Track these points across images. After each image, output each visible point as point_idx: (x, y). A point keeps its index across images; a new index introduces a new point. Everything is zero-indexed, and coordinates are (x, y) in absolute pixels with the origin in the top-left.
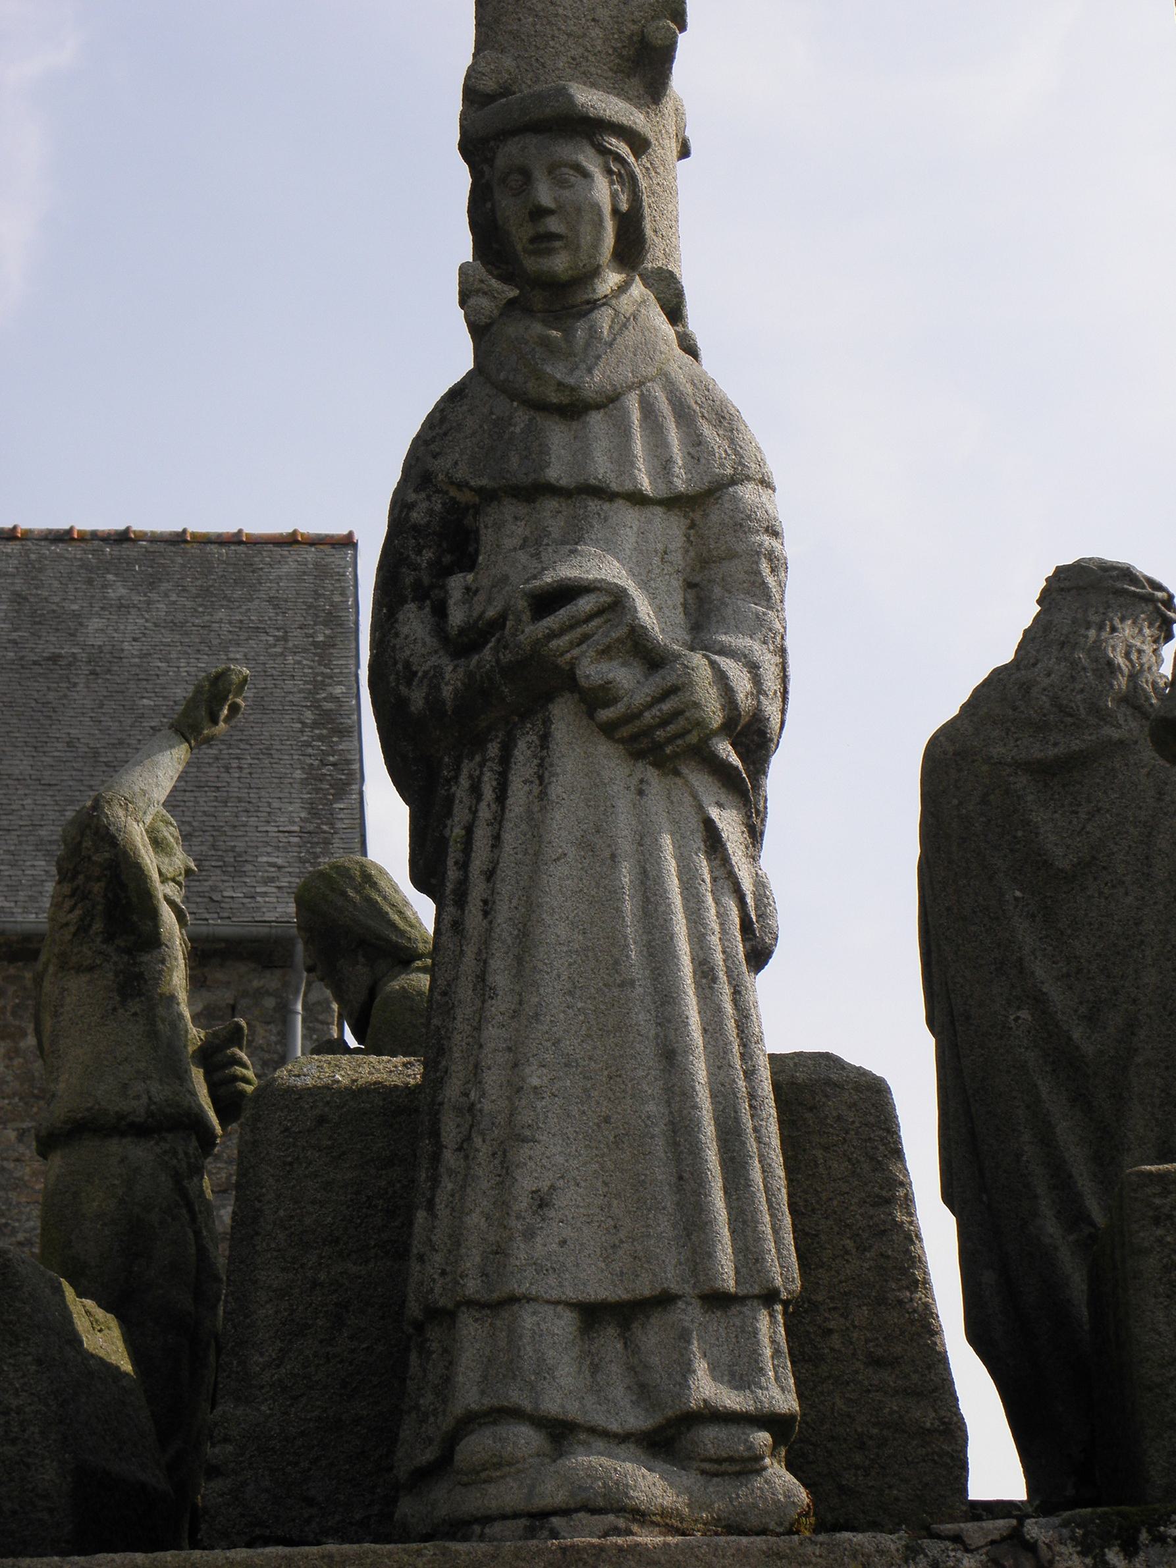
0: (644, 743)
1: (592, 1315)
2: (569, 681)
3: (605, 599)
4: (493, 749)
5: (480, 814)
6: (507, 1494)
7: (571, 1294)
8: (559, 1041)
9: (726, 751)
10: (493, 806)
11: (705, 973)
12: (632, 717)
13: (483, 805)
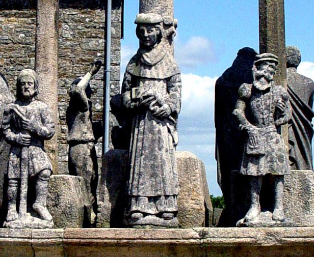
1: (150, 199)
3: (153, 97)
7: (147, 196)
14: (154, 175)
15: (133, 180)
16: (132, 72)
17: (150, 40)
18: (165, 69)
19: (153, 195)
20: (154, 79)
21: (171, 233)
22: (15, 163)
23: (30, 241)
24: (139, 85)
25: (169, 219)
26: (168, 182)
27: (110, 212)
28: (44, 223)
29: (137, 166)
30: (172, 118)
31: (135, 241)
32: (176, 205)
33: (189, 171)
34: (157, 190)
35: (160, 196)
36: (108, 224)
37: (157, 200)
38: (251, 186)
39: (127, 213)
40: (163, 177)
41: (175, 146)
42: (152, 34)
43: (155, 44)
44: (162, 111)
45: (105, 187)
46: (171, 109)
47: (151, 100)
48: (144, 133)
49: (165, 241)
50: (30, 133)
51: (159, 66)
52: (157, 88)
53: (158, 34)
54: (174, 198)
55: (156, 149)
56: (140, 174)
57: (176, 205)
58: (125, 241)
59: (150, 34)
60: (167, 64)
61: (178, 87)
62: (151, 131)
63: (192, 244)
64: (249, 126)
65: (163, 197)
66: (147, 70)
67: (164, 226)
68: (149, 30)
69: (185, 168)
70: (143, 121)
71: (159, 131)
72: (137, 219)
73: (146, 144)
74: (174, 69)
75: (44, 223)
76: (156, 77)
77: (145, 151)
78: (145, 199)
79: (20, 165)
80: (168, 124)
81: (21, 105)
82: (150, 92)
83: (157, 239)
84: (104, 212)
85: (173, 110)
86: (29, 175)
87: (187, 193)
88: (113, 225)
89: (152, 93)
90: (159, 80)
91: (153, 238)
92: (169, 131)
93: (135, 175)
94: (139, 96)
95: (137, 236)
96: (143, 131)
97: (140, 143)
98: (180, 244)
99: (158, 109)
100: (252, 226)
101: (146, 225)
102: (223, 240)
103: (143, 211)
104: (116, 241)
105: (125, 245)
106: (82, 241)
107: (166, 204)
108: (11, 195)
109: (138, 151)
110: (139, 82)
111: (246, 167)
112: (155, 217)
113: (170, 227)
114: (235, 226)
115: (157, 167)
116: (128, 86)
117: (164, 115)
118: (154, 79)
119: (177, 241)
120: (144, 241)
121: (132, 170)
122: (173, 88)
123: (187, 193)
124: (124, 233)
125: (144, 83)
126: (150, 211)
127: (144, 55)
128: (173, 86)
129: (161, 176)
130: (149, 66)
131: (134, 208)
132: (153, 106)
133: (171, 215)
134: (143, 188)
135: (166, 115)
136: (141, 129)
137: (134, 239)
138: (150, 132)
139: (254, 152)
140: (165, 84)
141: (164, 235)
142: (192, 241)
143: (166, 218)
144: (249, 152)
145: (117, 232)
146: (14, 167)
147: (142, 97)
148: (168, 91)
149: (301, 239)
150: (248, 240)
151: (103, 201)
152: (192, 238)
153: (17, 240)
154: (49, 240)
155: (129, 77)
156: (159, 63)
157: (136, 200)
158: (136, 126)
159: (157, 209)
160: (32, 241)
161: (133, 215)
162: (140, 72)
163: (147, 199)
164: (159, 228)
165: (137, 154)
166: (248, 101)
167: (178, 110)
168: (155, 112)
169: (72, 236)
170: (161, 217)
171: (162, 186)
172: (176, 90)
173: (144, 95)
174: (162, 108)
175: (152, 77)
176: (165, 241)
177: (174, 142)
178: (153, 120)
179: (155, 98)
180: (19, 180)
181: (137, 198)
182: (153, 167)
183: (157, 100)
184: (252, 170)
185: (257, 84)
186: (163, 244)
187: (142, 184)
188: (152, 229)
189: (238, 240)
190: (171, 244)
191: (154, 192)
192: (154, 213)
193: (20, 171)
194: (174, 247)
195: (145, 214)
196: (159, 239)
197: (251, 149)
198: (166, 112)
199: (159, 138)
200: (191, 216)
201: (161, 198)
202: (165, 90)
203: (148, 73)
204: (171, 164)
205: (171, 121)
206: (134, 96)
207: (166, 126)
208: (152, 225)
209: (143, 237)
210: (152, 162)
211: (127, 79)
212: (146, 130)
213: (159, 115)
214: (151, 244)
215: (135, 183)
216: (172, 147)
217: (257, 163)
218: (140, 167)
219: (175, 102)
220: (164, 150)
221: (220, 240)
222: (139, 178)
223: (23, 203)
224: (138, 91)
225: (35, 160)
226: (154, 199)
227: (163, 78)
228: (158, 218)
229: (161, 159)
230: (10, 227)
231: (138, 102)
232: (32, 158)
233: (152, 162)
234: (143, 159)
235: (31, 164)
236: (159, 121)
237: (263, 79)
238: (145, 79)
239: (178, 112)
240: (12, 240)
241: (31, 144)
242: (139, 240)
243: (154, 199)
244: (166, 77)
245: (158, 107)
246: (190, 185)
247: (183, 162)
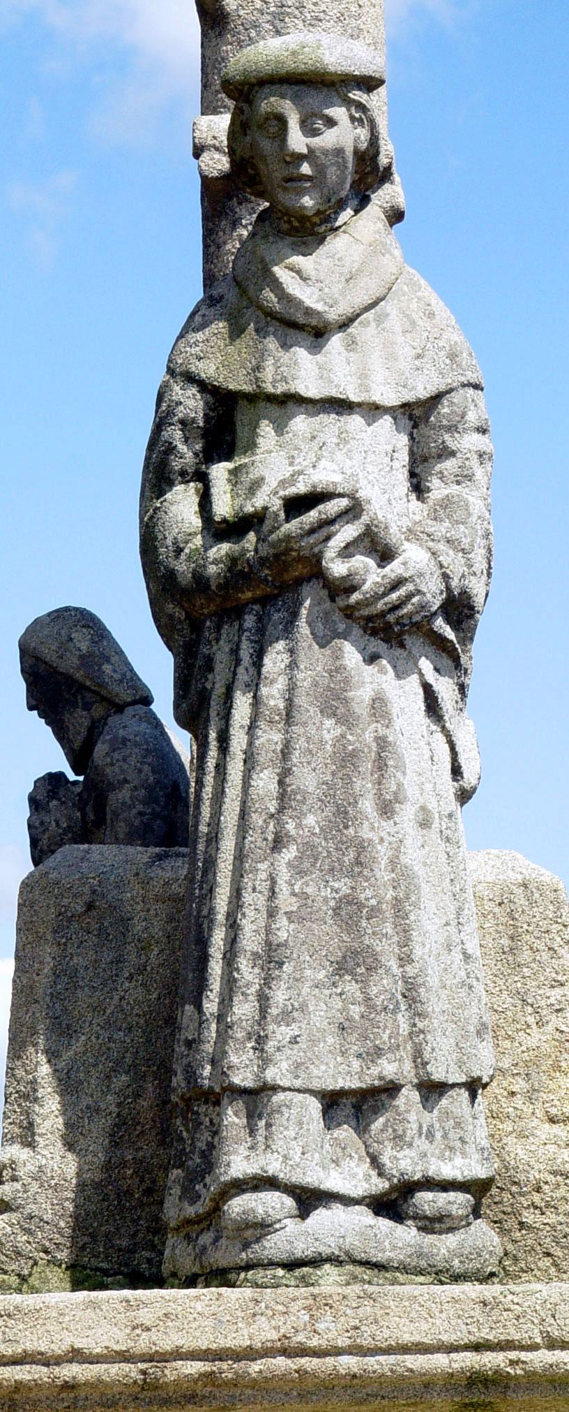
0: (379, 623)
1: (332, 1102)
2: (317, 572)
3: (344, 503)
4: (249, 621)
5: (239, 676)
6: (274, 1246)
7: (316, 1085)
8: (427, 1063)
9: (441, 625)
10: (251, 670)
11: (240, 856)
12: (367, 603)
13: (241, 670)
14: (353, 963)
15: (232, 1001)
16: (208, 369)
17: (317, 180)
18: (405, 352)
19: (354, 1084)
20: (340, 406)
21: (477, 1312)
24: (251, 446)
25: (451, 1230)
26: (436, 1003)
27: (70, 1206)
29: (250, 912)
30: (450, 634)
31: (255, 1367)
32: (485, 1143)
33: (526, 956)
34: (378, 1052)
35: (391, 1089)
36: (57, 1275)
37: (376, 1111)
39: (190, 1195)
40: (410, 970)
41: (464, 796)
42: (328, 139)
43: (341, 205)
44: (397, 584)
45: (42, 1058)
46: (446, 577)
47: (331, 522)
48: (289, 714)
49: (440, 1361)
51: (372, 330)
52: (358, 457)
53: (363, 146)
54: (473, 1096)
55: (368, 805)
56: (271, 957)
57: (485, 1143)
58: (194, 1368)
59: (316, 141)
60: (413, 323)
61: (474, 462)
62: (335, 701)
65: (409, 1097)
66: (301, 353)
67: (421, 1272)
68: (314, 115)
69: (505, 942)
70: (280, 645)
71: (379, 707)
72: (263, 1227)
73: (307, 779)
74: (453, 356)
76: (354, 398)
77: (300, 817)
78: (303, 1106)
80: (426, 665)
82: (324, 475)
83: (388, 1351)
84: (31, 1208)
85: (454, 583)
87: (519, 1085)
88: (85, 1276)
89: (337, 478)
90: (373, 410)
91: (366, 1342)
92: (432, 705)
93: (243, 963)
94: (260, 500)
95: (265, 1332)
96: (282, 705)
97: (265, 774)
98: (530, 1375)
99: (371, 574)
101: (315, 1262)
103: (297, 1178)
104: (132, 1371)
107: (430, 1136)
109: (257, 820)
110: (257, 426)
112: (363, 1217)
113: (457, 1278)
115: (374, 912)
116: (186, 454)
117: (408, 608)
118: (340, 406)
119: (513, 1363)
120: (307, 1363)
121: (218, 938)
122: (449, 465)
123: (519, 1085)
124: (183, 1321)
125: (280, 429)
126: (333, 1181)
127: (277, 270)
128: (449, 453)
129: (393, 964)
130: (314, 331)
132: (347, 552)
133: (458, 1202)
134: (294, 1041)
135: (422, 607)
136: (273, 694)
137: (250, 1354)
138: (328, 710)
140: (403, 440)
141: (426, 1323)
143: (433, 1224)
145: (145, 1316)
147: (276, 505)
148: (418, 488)
151: (30, 1144)
155: (191, 403)
156: (369, 315)
157: (252, 1116)
158: (243, 676)
159: (375, 1161)
161: (238, 1205)
162: (258, 368)
163: (315, 1106)
164: (394, 1282)
165: (252, 838)
167: (477, 588)
168: (354, 588)
170: (399, 1217)
171: (404, 1028)
172: (464, 477)
173: (291, 491)
174: (395, 569)
175: (334, 393)
176: (440, 1361)
177: (456, 771)
178: (345, 636)
179: (354, 510)
181: (256, 1098)
183: (365, 518)
186: (427, 1384)
187: (286, 1017)
188: (357, 1288)
190: (476, 1380)
191: (356, 1064)
192: (358, 1191)
194: (492, 1397)
195: (309, 1199)
196: (405, 1349)
198: (419, 592)
199: (382, 743)
200: (552, 1218)
201: (400, 1101)
202: (402, 476)
203: (305, 371)
204: (448, 898)
205: (440, 644)
206: (223, 507)
207: (415, 678)
208: (355, 1262)
209: (301, 1338)
210: (343, 886)
211: (181, 412)
212: (301, 700)
213: (380, 605)
214: (354, 1385)
215: (244, 1009)
216: (452, 804)
218: (272, 914)
219: (466, 542)
220: (407, 814)
222: (267, 981)
224: (246, 479)
226: (354, 1107)
227: (390, 397)
228: (384, 1224)
229: (393, 863)
231: (252, 536)
233: (343, 886)
234: (289, 864)
236: (377, 645)
238: (290, 402)
239: (478, 600)
242: (281, 1363)
243: (354, 1107)
244: (409, 397)
245: (371, 563)
246: (535, 1038)
247: (489, 906)
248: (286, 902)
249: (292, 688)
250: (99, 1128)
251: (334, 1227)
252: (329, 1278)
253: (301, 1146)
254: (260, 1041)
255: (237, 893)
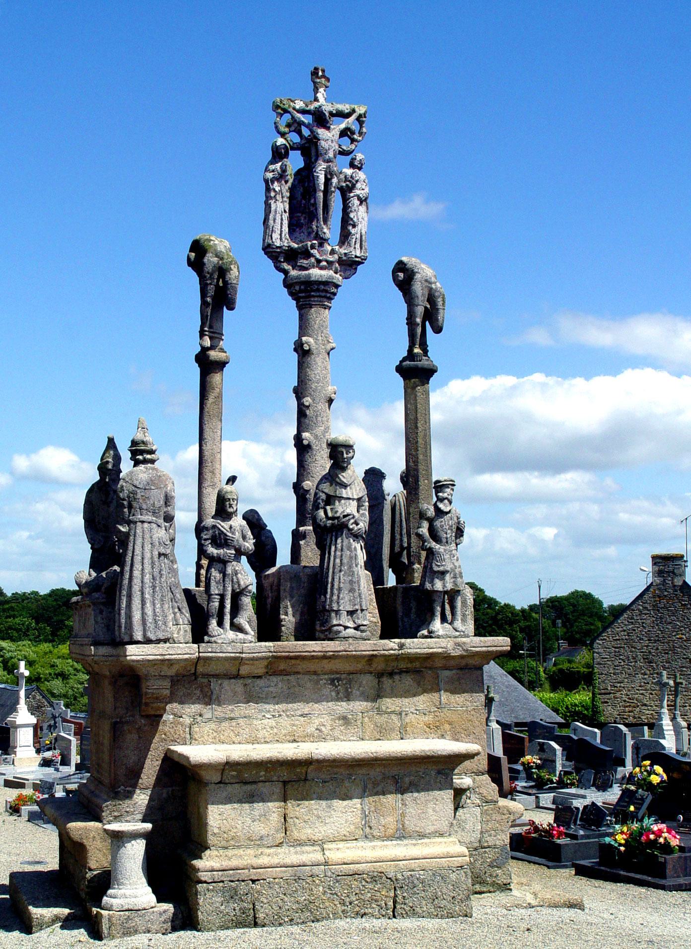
6: (341, 635)
11: (333, 572)
20: (349, 499)
22: (218, 578)
23: (241, 655)
28: (249, 637)
36: (293, 638)
38: (434, 601)
48: (342, 550)
50: (236, 550)
56: (340, 589)
63: (391, 655)
64: (433, 544)
71: (355, 548)
72: (340, 632)
73: (345, 561)
75: (249, 637)
79: (224, 581)
81: (223, 521)
86: (233, 591)
88: (297, 639)
90: (353, 499)
94: (338, 515)
95: (342, 648)
100: (438, 637)
102: (418, 650)
105: (330, 657)
106: (291, 654)
108: (214, 611)
111: (432, 582)
114: (417, 637)
118: (349, 499)
121: (329, 585)
130: (345, 486)
131: (335, 622)
136: (339, 546)
139: (441, 569)
142: (392, 652)
143: (362, 631)
144: (436, 569)
146: (217, 583)
149: (484, 649)
150: (440, 650)
152: (392, 649)
153: (229, 655)
154: (260, 655)
155: (323, 496)
158: (333, 542)
159: (354, 622)
160: (244, 655)
161: (335, 628)
166: (431, 521)
169: (281, 650)
179: (354, 517)
180: (222, 597)
181: (337, 612)
182: (351, 582)
184: (438, 585)
185: (441, 506)
189: (431, 650)
190: (373, 655)
193: (224, 586)
197: (438, 566)
203: (344, 493)
215: (335, 597)
217: (443, 579)
221: (415, 651)
223: (227, 618)
225: (239, 575)
226: (351, 613)
227: (356, 497)
230: (216, 642)
232: (236, 574)
235: (235, 580)
237: (446, 501)
240: (224, 655)
241: (234, 560)
243: (351, 613)
248: (342, 580)
249: (342, 546)
250: (298, 613)
251: (351, 632)
252: (350, 640)
253: (345, 620)
254: (338, 603)
255: (333, 579)
